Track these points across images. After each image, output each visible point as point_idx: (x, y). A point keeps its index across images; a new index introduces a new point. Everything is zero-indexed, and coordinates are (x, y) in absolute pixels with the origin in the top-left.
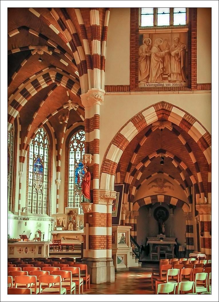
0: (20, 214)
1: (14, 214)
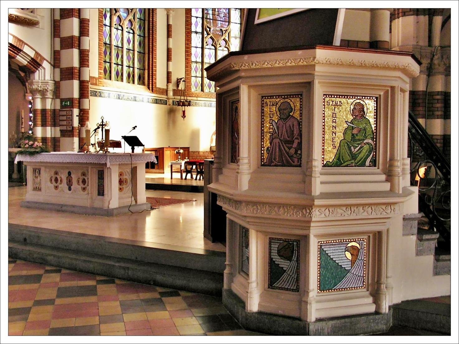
0: (171, 94)
1: (152, 91)
